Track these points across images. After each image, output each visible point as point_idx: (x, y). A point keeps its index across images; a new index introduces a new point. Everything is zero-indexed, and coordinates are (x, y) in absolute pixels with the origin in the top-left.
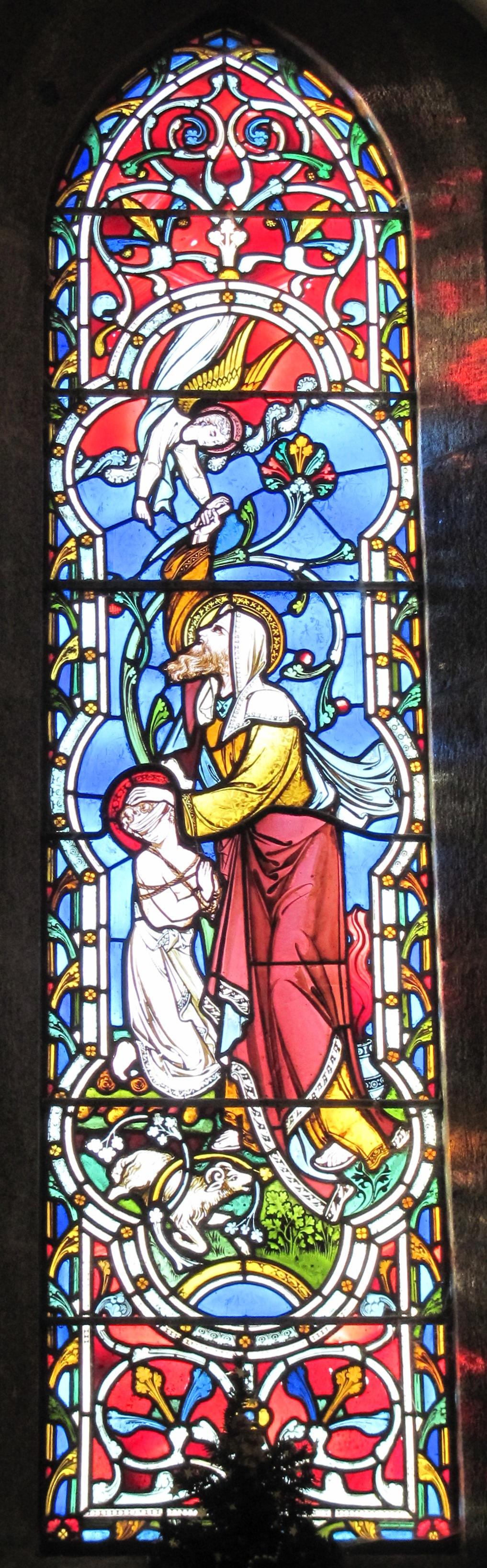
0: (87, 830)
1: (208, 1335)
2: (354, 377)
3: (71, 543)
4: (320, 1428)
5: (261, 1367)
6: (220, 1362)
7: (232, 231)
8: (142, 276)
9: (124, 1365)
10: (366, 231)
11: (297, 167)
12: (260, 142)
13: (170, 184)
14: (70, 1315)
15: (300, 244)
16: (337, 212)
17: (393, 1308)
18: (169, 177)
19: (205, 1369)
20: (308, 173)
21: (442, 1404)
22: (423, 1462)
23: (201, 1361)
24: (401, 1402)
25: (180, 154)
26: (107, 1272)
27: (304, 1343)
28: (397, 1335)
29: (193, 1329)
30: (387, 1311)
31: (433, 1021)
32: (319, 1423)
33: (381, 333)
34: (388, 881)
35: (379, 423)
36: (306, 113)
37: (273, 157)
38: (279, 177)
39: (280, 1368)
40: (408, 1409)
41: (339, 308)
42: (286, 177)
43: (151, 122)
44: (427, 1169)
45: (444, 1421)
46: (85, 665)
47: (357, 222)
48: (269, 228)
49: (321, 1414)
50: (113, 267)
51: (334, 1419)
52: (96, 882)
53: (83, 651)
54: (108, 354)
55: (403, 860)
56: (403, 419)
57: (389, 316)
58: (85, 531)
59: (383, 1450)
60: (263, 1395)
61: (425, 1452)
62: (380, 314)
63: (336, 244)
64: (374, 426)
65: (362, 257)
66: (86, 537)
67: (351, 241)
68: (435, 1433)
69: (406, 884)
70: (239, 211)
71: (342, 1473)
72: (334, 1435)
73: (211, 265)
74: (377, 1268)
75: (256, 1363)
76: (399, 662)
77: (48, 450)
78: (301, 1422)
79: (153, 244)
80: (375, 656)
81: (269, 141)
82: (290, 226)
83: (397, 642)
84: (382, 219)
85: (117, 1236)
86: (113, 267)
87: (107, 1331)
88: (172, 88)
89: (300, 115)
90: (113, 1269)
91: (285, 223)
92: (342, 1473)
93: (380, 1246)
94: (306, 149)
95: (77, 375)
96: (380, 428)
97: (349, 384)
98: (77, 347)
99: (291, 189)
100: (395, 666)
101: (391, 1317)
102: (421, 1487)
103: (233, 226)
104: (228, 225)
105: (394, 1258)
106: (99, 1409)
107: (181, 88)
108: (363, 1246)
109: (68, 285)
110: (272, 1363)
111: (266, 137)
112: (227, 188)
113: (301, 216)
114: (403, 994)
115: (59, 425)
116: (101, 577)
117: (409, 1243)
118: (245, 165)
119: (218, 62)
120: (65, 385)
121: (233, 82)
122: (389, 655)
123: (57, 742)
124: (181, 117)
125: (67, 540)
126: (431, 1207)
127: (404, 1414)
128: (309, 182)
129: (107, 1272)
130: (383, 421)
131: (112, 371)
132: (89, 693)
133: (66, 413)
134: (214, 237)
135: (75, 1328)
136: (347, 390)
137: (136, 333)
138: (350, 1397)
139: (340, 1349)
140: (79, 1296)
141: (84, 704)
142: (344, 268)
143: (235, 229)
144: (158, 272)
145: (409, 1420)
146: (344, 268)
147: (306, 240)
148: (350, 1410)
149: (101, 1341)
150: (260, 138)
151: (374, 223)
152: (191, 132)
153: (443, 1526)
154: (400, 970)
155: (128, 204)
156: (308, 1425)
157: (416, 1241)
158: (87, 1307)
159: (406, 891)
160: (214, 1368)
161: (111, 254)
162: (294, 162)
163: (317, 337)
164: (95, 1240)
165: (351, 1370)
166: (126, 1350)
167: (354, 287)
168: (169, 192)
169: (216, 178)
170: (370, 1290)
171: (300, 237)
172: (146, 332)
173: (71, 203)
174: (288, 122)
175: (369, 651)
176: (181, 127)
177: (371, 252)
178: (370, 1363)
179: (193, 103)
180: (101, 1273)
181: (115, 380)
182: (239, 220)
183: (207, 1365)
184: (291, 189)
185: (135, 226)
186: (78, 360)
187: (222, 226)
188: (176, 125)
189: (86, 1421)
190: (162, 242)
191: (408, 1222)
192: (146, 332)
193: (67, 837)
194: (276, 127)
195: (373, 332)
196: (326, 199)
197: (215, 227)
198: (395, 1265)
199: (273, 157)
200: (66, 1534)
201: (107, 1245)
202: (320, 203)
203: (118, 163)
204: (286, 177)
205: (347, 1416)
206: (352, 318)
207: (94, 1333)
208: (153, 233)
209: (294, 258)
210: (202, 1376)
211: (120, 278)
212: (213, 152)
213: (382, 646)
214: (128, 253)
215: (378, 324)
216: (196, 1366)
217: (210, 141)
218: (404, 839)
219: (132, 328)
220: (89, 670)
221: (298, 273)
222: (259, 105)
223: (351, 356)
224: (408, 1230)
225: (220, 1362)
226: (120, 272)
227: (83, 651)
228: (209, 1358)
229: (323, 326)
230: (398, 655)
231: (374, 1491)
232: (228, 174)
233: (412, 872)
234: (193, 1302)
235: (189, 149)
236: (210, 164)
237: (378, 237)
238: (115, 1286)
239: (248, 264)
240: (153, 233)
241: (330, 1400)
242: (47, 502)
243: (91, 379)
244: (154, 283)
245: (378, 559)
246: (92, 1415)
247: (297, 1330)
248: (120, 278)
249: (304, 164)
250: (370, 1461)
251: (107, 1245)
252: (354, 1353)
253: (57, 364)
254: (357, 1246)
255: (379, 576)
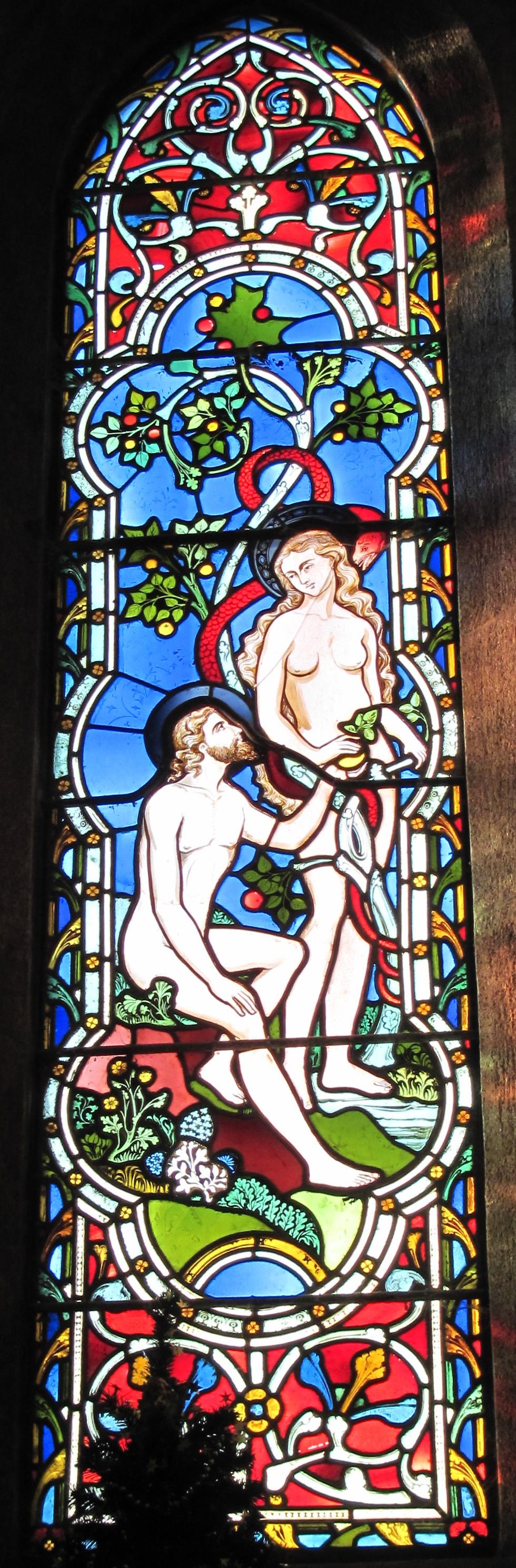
0: (94, 794)
1: (211, 1322)
2: (381, 322)
3: (83, 507)
4: (339, 1418)
5: (274, 1356)
6: (224, 1350)
7: (253, 196)
8: (165, 246)
9: (120, 1356)
10: (394, 182)
11: (322, 131)
12: (284, 111)
13: (190, 158)
14: (60, 1299)
15: (326, 202)
16: (361, 167)
17: (422, 1281)
18: (189, 151)
19: (208, 1359)
20: (335, 137)
21: (477, 1394)
22: (454, 1457)
23: (205, 1349)
24: (430, 1386)
25: (202, 129)
26: (103, 1257)
27: (315, 1329)
28: (427, 1313)
29: (196, 1314)
30: (416, 1285)
31: (467, 969)
32: (336, 1412)
33: (408, 278)
34: (418, 824)
35: (407, 362)
36: (327, 78)
37: (296, 122)
38: (301, 143)
39: (295, 1354)
40: (438, 1396)
41: (363, 259)
42: (308, 143)
43: (173, 103)
44: (460, 1134)
45: (478, 1410)
46: (94, 627)
47: (382, 176)
48: (296, 187)
49: (338, 1405)
50: (132, 241)
51: (353, 1409)
52: (100, 845)
53: (90, 613)
54: (126, 324)
55: (435, 803)
56: (434, 361)
57: (417, 261)
58: (97, 493)
59: (409, 1440)
60: (274, 1386)
61: (457, 1447)
62: (408, 259)
63: (364, 198)
64: (400, 365)
65: (390, 205)
66: (99, 499)
67: (378, 194)
68: (469, 1424)
69: (438, 828)
70: (263, 177)
71: (364, 1468)
72: (356, 1427)
73: (231, 229)
74: (405, 1242)
75: (265, 1351)
76: (429, 595)
77: (43, 1130)
78: (317, 1413)
79: (172, 215)
80: (402, 592)
81: (289, 110)
82: (314, 187)
83: (426, 576)
84: (410, 171)
85: (116, 1219)
86: (132, 241)
87: (103, 1320)
88: (197, 68)
89: (322, 83)
90: (110, 1254)
91: (307, 183)
92: (364, 1468)
93: (409, 1218)
94: (329, 113)
95: (93, 344)
96: (408, 367)
97: (378, 329)
98: (94, 319)
99: (311, 153)
100: (424, 599)
101: (421, 1292)
102: (454, 1489)
103: (255, 191)
104: (249, 191)
105: (424, 1233)
106: (89, 1406)
107: (204, 68)
108: (390, 1218)
109: (86, 260)
110: (286, 1349)
111: (288, 106)
112: (249, 157)
113: (324, 175)
114: (433, 941)
115: (73, 393)
116: (112, 534)
117: (441, 1218)
118: (267, 134)
119: (242, 40)
120: (81, 356)
121: (256, 57)
122: (418, 591)
123: (65, 702)
124: (202, 95)
125: (78, 503)
126: (464, 1177)
127: (433, 1403)
128: (333, 144)
129: (103, 1257)
130: (410, 359)
131: (131, 340)
132: (97, 655)
133: (80, 381)
134: (236, 203)
135: (66, 1316)
136: (376, 336)
137: (157, 299)
138: (370, 1383)
139: (363, 1332)
140: (72, 1280)
141: (91, 665)
142: (370, 221)
143: (256, 194)
144: (179, 241)
145: (438, 1409)
146: (370, 221)
147: (332, 198)
148: (373, 1399)
149: (95, 1331)
150: (281, 108)
151: (400, 177)
152: (213, 109)
153: (482, 1529)
154: (430, 917)
155: (149, 180)
156: (325, 1415)
157: (448, 1214)
158: (80, 1292)
159: (440, 835)
160: (218, 1356)
161: (130, 229)
162: (317, 127)
163: (296, 263)
164: (89, 1221)
165: (372, 1353)
166: (121, 1341)
167: (380, 239)
168: (189, 165)
169: (237, 150)
170: (396, 1265)
171: (325, 195)
172: (167, 296)
173: (90, 185)
174: (311, 92)
175: (396, 589)
176: (203, 104)
177: (398, 202)
178: (396, 1346)
179: (215, 81)
180: (97, 1258)
181: (134, 348)
182: (261, 185)
183: (211, 1352)
184: (311, 153)
185: (154, 200)
186: (95, 329)
187: (244, 192)
188: (198, 102)
189: (76, 1415)
190: (181, 212)
191: (440, 1192)
192: (167, 296)
193: (71, 803)
194: (297, 94)
195: (401, 278)
196: (350, 158)
197: (238, 193)
198: (424, 1241)
199: (296, 122)
200: (52, 1545)
201: (104, 1228)
202: (344, 163)
203: (139, 142)
204: (308, 143)
205: (368, 1405)
206: (378, 268)
207: (87, 1324)
208: (173, 207)
209: (318, 215)
210: (207, 1366)
211: (139, 253)
212: (236, 124)
213: (410, 581)
214: (147, 228)
215: (405, 270)
216: (198, 1355)
217: (231, 116)
218: (435, 782)
219: (154, 294)
220: (97, 632)
221: (323, 229)
222: (281, 75)
223: (377, 303)
224: (439, 1202)
225: (224, 1350)
226: (138, 246)
227: (90, 613)
228: (212, 1346)
229: (346, 276)
230: (426, 588)
231: (403, 1488)
232: (248, 139)
233: (445, 814)
234: (198, 1286)
235: (209, 123)
236: (232, 136)
237: (405, 191)
238: (112, 1273)
239: (268, 226)
240: (173, 207)
241: (348, 1387)
242: (62, 469)
243: (109, 347)
244: (174, 251)
245: (407, 496)
246: (81, 1408)
247: (311, 1313)
248: (139, 253)
249: (329, 128)
250: (393, 1456)
251: (104, 1228)
252: (377, 1335)
253: (72, 336)
254: (383, 1218)
255: (408, 513)
